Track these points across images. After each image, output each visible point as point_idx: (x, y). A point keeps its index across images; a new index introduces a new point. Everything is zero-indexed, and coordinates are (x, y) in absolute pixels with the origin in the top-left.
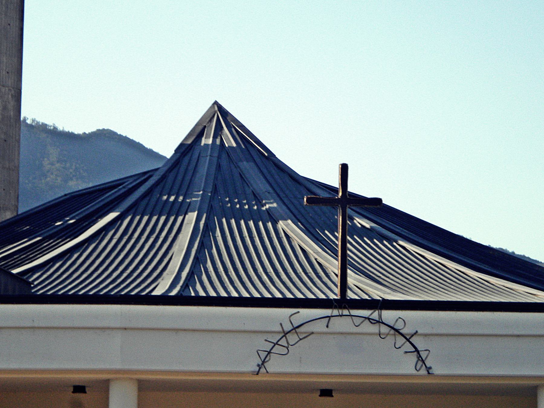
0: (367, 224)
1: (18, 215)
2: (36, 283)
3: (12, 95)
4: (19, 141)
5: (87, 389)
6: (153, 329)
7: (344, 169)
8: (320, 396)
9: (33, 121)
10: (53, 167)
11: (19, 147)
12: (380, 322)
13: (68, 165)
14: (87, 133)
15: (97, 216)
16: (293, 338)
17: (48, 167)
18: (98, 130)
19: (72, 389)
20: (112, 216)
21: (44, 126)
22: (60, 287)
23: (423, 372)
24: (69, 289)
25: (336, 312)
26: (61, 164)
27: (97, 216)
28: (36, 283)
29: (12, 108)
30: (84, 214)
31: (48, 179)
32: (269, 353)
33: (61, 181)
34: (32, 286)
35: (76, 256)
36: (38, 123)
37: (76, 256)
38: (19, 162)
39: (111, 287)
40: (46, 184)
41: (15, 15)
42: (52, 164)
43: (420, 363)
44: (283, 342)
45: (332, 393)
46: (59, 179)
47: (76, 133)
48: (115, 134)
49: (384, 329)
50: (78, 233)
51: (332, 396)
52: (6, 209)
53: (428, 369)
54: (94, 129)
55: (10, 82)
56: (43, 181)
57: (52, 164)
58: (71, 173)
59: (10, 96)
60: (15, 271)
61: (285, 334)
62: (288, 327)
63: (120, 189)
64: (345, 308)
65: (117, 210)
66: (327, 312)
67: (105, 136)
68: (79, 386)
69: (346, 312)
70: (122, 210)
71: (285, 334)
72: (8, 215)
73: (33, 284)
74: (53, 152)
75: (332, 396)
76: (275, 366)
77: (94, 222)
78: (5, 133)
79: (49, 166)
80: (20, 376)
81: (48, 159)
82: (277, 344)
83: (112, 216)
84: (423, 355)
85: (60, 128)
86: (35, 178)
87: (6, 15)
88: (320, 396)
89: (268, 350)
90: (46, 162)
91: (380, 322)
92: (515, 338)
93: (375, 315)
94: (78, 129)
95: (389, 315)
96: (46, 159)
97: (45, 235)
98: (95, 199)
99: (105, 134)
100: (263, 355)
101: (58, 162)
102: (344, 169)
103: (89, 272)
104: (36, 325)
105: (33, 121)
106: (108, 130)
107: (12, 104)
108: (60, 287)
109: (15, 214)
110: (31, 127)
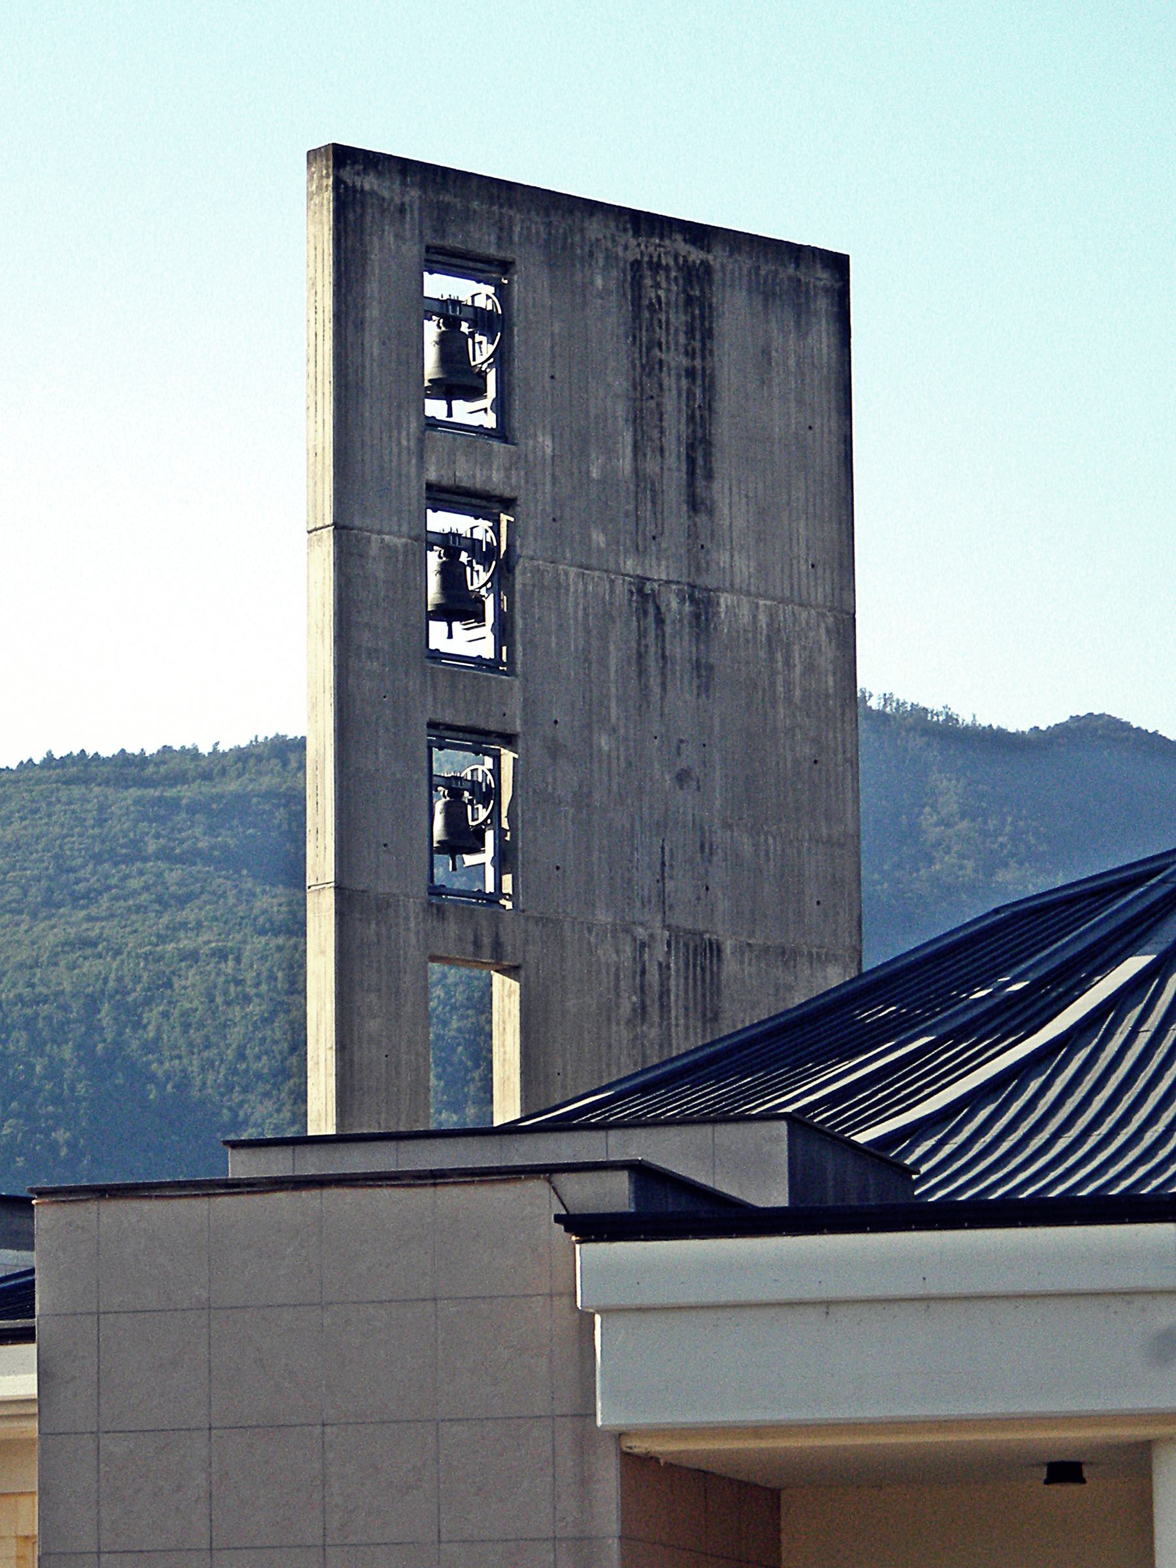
1: (861, 975)
2: (924, 1169)
3: (828, 631)
4: (854, 763)
5: (1086, 1472)
6: (680, 1308)
7: (450, 636)
8: (1047, 1482)
9: (887, 700)
10: (950, 831)
11: (856, 779)
13: (992, 824)
14: (1043, 728)
15: (1090, 968)
17: (934, 833)
18: (1075, 719)
19: (1043, 1473)
20: (1134, 965)
21: (920, 713)
22: (993, 1178)
24: (1019, 1182)
26: (973, 820)
27: (1090, 968)
28: (924, 1169)
29: (830, 668)
30: (1057, 961)
31: (938, 867)
33: (975, 871)
34: (914, 1177)
35: (1034, 1085)
36: (900, 705)
37: (1034, 1085)
38: (857, 819)
39: (1141, 1171)
40: (937, 881)
41: (825, 400)
42: (946, 823)
45: (1080, 1472)
46: (969, 864)
47: (1012, 730)
48: (1125, 726)
50: (1037, 1021)
51: (1083, 1481)
52: (821, 959)
54: (1061, 717)
55: (820, 594)
56: (922, 872)
57: (946, 823)
58: (1002, 845)
59: (823, 631)
60: (862, 1138)
63: (1153, 887)
65: (1147, 948)
67: (1095, 734)
68: (1062, 1464)
70: (1162, 947)
72: (834, 977)
73: (918, 1172)
74: (949, 789)
75: (1083, 1481)
77: (1082, 987)
78: (816, 741)
79: (938, 829)
80: (860, 1441)
81: (934, 807)
83: (1134, 965)
85: (965, 718)
86: (899, 866)
87: (800, 402)
88: (1047, 1482)
90: (928, 819)
92: (879, 1307)
94: (1017, 721)
96: (927, 809)
97: (943, 1030)
98: (1084, 919)
99: (1096, 729)
101: (963, 816)
102: (450, 636)
103: (1104, 1129)
104: (934, 1291)
105: (887, 700)
106: (1102, 716)
107: (827, 656)
108: (993, 1178)
109: (854, 973)
110: (881, 716)
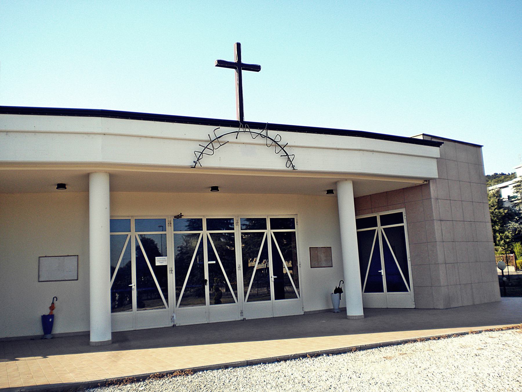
0: (117, 298)
8: (57, 188)
12: (267, 137)
16: (216, 145)
23: (291, 169)
25: (241, 130)
32: (202, 153)
43: (289, 162)
44: (210, 146)
49: (269, 142)
51: (66, 188)
53: (293, 166)
61: (211, 142)
62: (213, 138)
64: (247, 128)
66: (237, 129)
69: (247, 130)
71: (211, 142)
75: (66, 188)
76: (208, 162)
82: (206, 147)
84: (291, 158)
88: (57, 188)
89: (243, 61)
91: (267, 137)
93: (264, 132)
95: (272, 133)
100: (198, 154)
